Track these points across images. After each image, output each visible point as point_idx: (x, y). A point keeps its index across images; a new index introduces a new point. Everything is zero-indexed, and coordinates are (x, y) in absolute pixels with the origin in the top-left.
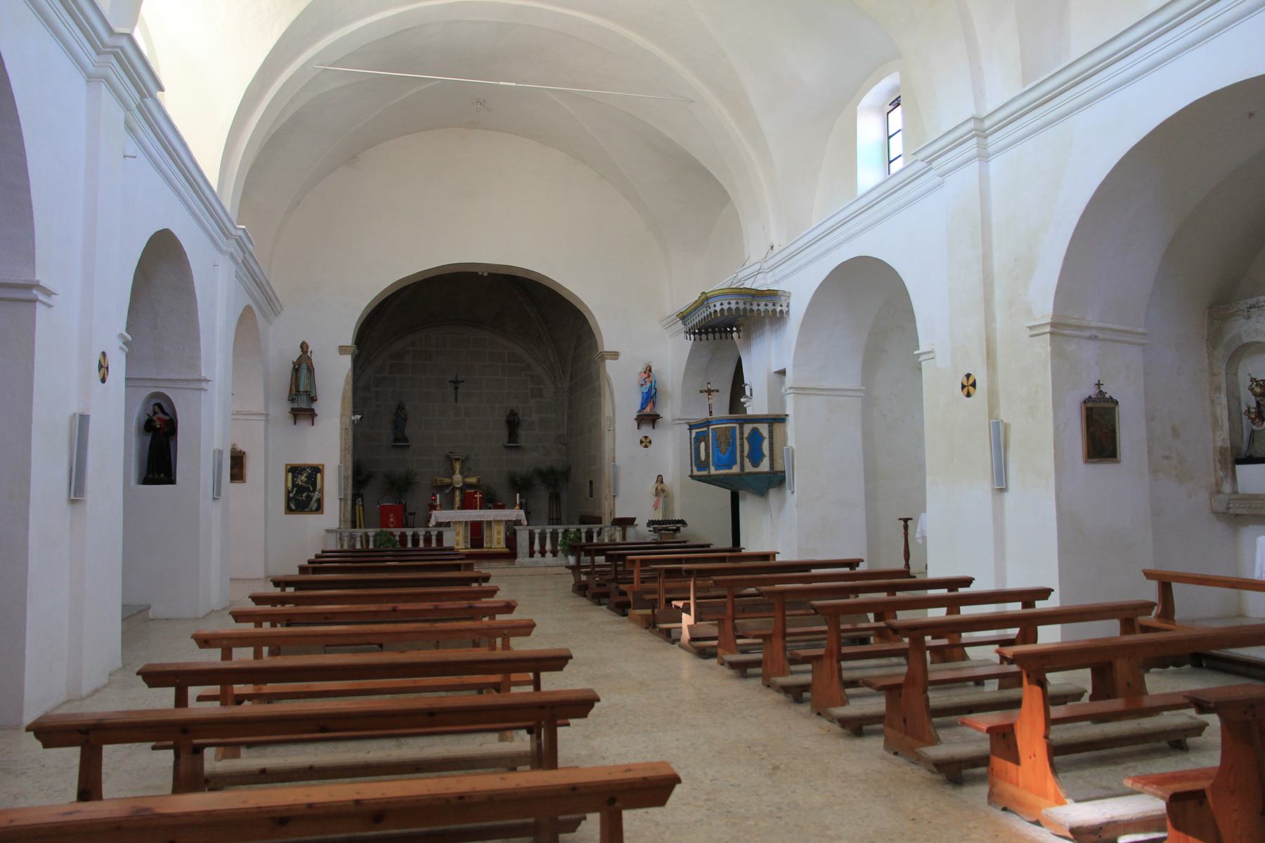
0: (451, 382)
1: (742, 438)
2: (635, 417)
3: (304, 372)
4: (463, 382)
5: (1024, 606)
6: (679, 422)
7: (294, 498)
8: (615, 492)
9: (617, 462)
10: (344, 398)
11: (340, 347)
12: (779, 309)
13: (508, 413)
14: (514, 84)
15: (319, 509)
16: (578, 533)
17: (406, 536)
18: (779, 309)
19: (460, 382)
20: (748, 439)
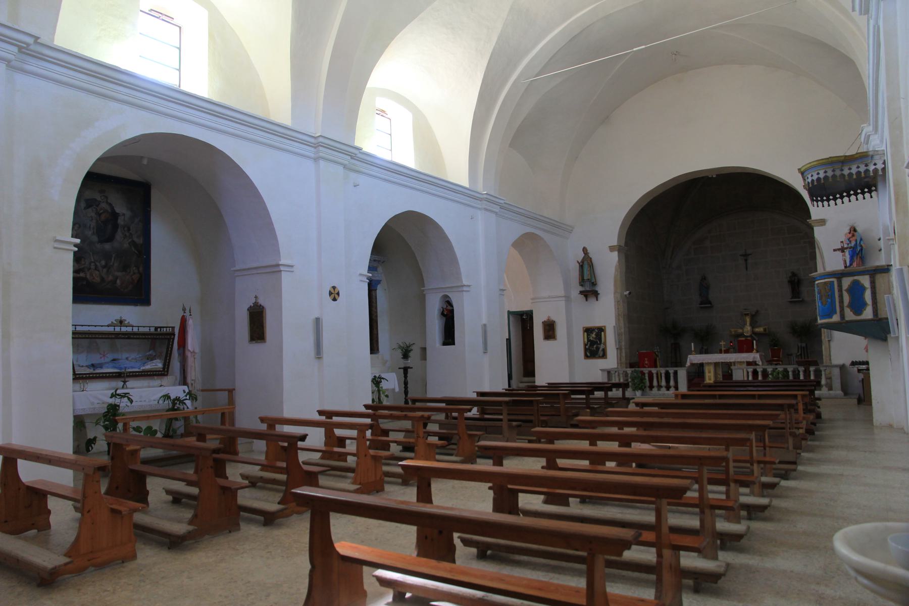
0: (741, 255)
1: (840, 290)
3: (586, 267)
4: (751, 254)
5: (591, 444)
7: (589, 349)
11: (610, 247)
12: (872, 168)
13: (790, 275)
14: (643, 47)
15: (604, 356)
18: (872, 168)
20: (848, 291)
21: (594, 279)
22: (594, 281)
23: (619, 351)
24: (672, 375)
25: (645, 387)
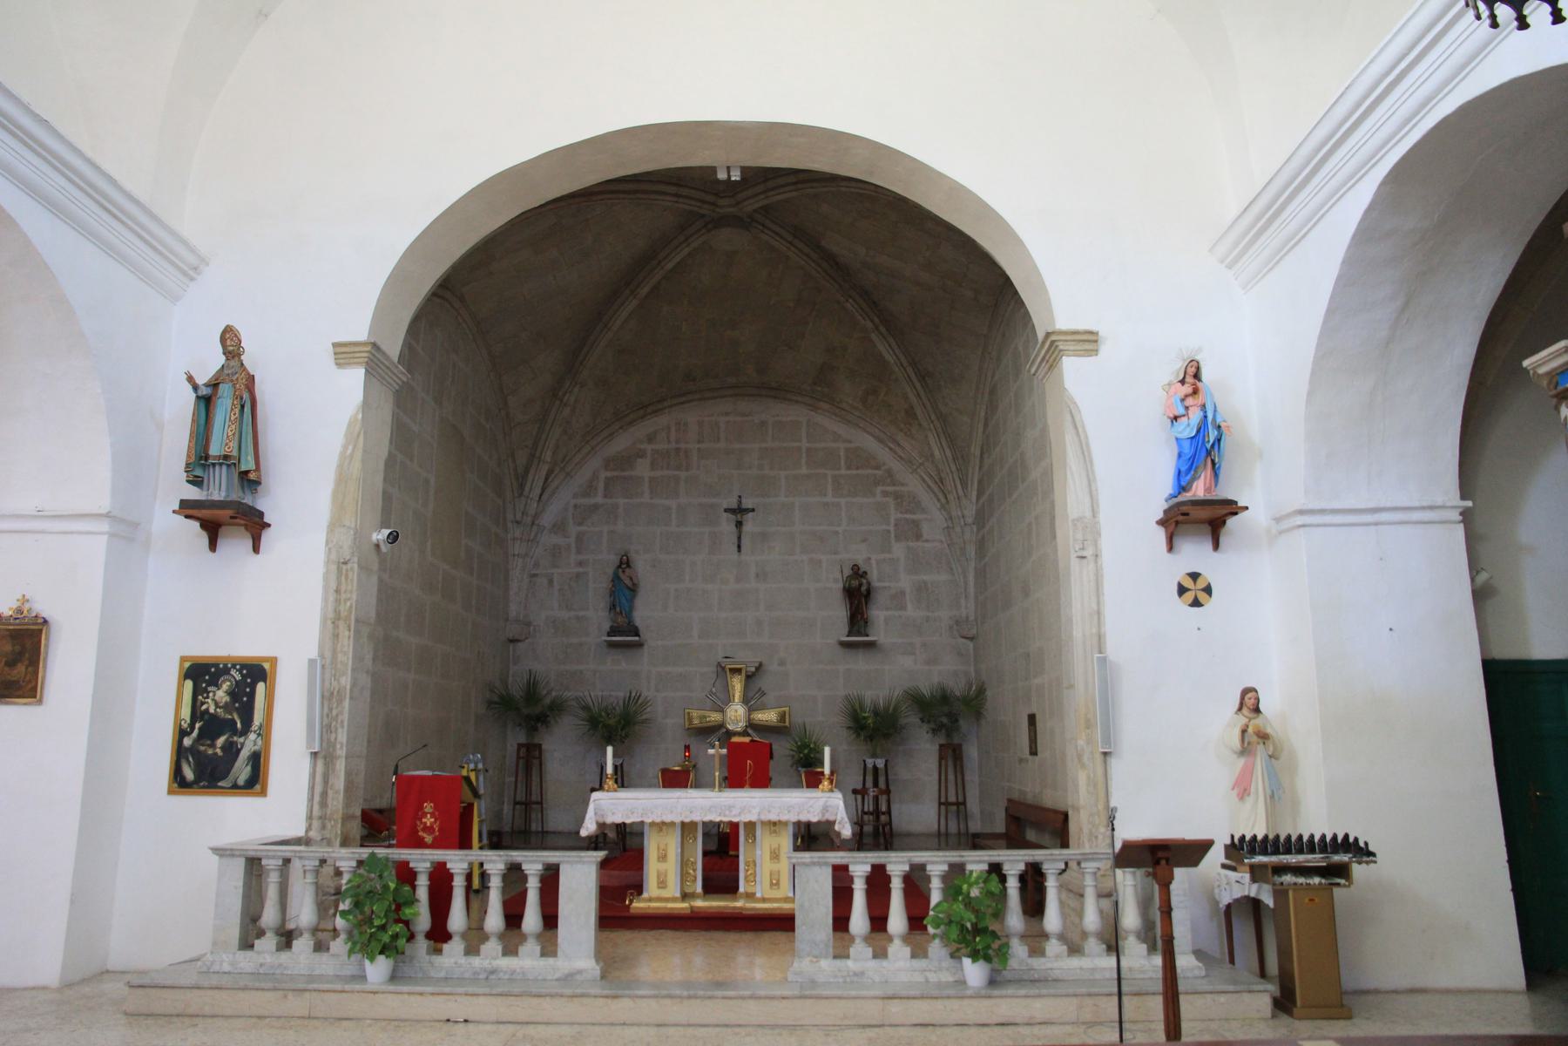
0: (726, 510)
2: (1160, 515)
6: (1300, 520)
7: (192, 750)
8: (1107, 739)
9: (1113, 649)
10: (341, 479)
11: (335, 345)
13: (848, 572)
15: (255, 782)
16: (994, 877)
17: (450, 877)
21: (251, 458)
22: (252, 466)
23: (320, 764)
24: (533, 885)
25: (411, 937)
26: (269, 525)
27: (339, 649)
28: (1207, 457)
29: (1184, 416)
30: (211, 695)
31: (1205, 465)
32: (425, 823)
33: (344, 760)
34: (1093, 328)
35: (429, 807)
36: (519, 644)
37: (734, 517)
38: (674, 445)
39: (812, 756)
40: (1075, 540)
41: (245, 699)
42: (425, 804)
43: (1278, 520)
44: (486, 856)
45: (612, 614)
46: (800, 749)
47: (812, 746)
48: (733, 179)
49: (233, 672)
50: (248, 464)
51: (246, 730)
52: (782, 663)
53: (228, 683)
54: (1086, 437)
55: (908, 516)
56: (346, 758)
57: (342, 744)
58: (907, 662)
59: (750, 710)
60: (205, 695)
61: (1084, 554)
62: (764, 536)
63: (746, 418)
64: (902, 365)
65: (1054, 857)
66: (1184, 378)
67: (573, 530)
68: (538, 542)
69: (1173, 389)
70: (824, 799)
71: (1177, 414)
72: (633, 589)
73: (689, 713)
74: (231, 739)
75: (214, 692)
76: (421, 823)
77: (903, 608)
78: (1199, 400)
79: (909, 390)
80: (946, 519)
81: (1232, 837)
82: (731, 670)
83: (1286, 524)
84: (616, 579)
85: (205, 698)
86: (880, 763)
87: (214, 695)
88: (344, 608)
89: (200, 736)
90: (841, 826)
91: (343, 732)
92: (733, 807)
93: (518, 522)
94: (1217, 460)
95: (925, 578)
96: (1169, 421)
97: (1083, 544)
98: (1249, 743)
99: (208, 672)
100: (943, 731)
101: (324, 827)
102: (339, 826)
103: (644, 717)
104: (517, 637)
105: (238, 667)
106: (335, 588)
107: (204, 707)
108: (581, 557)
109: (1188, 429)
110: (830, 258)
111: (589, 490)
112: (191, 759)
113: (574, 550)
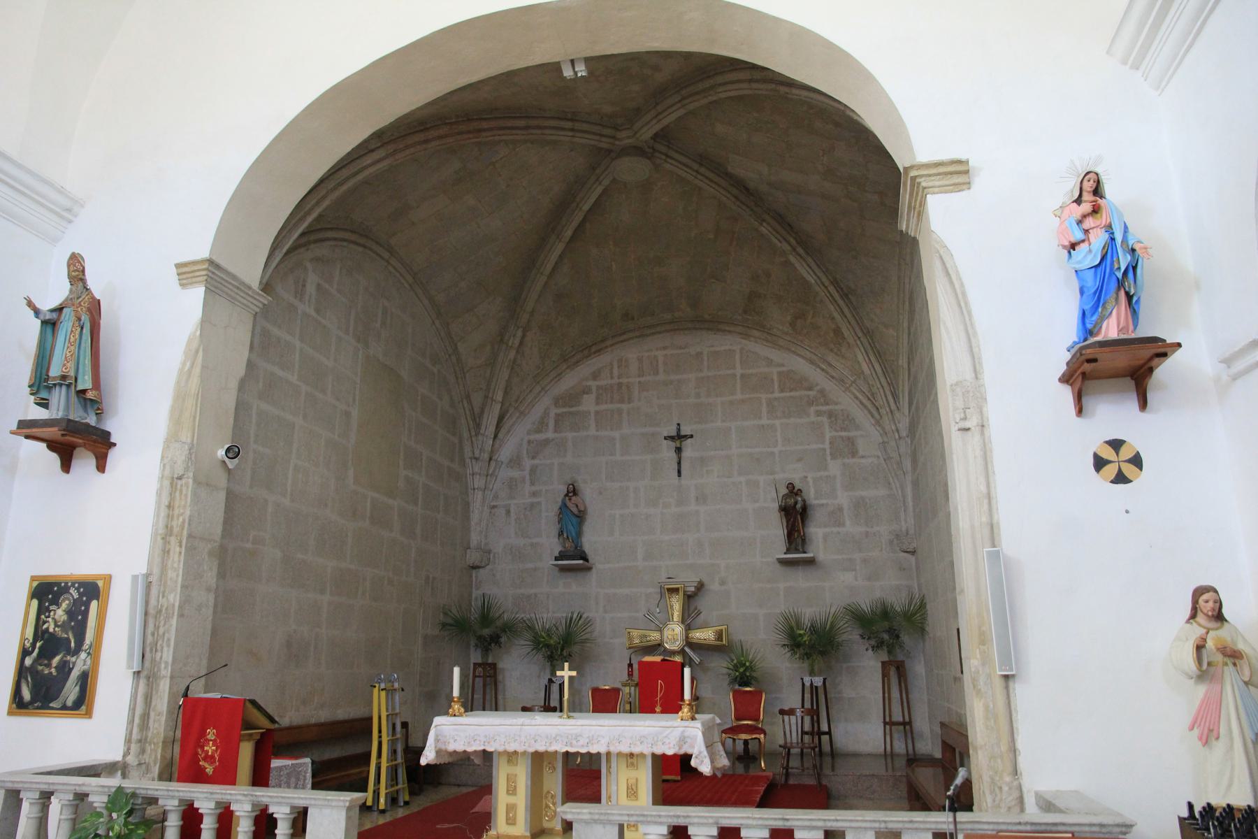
2: (1063, 368)
7: (32, 670)
8: (1006, 658)
9: (1008, 545)
10: (180, 396)
11: (178, 266)
13: (784, 491)
15: (82, 704)
19: (686, 437)
26: (114, 445)
27: (169, 565)
28: (1119, 289)
29: (1083, 241)
30: (52, 613)
31: (1117, 299)
32: (207, 751)
33: (168, 681)
34: (963, 158)
35: (211, 733)
36: (481, 570)
37: (674, 444)
38: (616, 380)
39: (748, 674)
40: (955, 409)
41: (80, 617)
42: (208, 730)
43: (1228, 361)
44: (231, 794)
45: (561, 540)
46: (736, 668)
47: (747, 664)
48: (579, 75)
49: (72, 590)
50: (85, 382)
51: (77, 652)
52: (723, 583)
53: (67, 602)
54: (962, 285)
55: (844, 434)
56: (172, 678)
57: (166, 663)
58: (847, 578)
59: (688, 628)
60: (47, 614)
61: (967, 424)
62: (702, 461)
63: (682, 351)
64: (824, 285)
65: (916, 825)
66: (1080, 195)
67: (528, 463)
68: (497, 477)
69: (1067, 211)
70: (681, 729)
71: (1073, 240)
72: (581, 516)
73: (629, 633)
74: (65, 659)
75: (55, 610)
76: (203, 750)
77: (842, 524)
78: (1103, 219)
79: (832, 308)
80: (881, 435)
81: (1191, 806)
82: (669, 590)
83: (1240, 365)
84: (564, 508)
85: (47, 617)
86: (818, 681)
87: (55, 614)
88: (176, 524)
89: (40, 656)
90: (698, 761)
91: (168, 651)
92: (580, 736)
93: (477, 459)
94: (1132, 292)
95: (864, 493)
96: (1066, 252)
97: (965, 412)
98: (1209, 664)
99: (51, 592)
100: (885, 648)
101: (143, 751)
102: (159, 751)
103: (584, 637)
104: (477, 563)
105: (77, 585)
106: (167, 503)
107: (45, 626)
108: (534, 488)
109: (1090, 257)
110: (742, 189)
111: (541, 426)
112: (29, 679)
113: (528, 482)
